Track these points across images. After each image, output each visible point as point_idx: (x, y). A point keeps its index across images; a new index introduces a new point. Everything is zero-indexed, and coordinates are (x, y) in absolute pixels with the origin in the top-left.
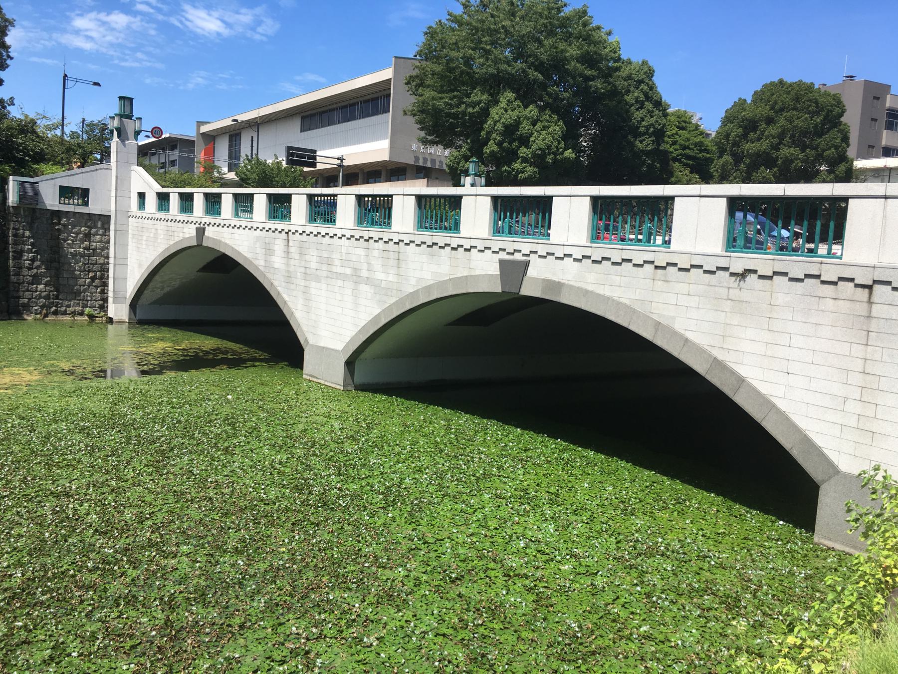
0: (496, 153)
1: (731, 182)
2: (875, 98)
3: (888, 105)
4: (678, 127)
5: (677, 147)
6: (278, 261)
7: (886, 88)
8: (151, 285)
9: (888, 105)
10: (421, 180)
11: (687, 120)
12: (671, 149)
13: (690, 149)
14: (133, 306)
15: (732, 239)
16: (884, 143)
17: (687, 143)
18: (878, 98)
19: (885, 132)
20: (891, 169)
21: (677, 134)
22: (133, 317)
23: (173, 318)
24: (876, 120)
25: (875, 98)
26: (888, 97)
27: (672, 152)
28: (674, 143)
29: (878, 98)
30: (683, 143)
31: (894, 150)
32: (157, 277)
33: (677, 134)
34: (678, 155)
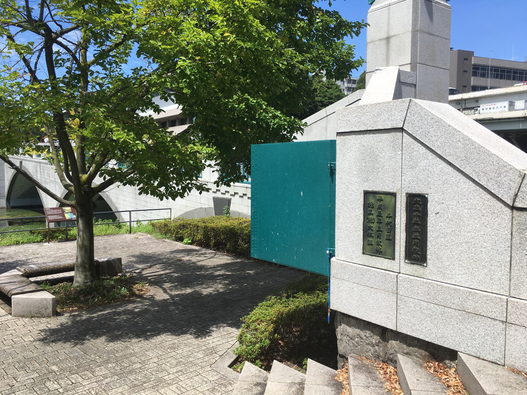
0: (108, 109)
1: (499, 159)
2: (465, 59)
3: (473, 63)
4: (327, 87)
5: (327, 98)
6: (39, 175)
7: (471, 53)
8: (14, 189)
9: (473, 63)
10: (522, 101)
11: (333, 83)
12: (323, 100)
13: (333, 99)
14: (8, 199)
15: (399, 373)
16: (472, 84)
17: (331, 96)
18: (467, 59)
19: (472, 78)
20: (465, 100)
21: (326, 91)
22: (8, 205)
23: (30, 204)
24: (466, 71)
25: (465, 59)
26: (473, 58)
27: (324, 101)
28: (325, 96)
29: (467, 59)
30: (329, 96)
31: (478, 88)
32: (15, 185)
33: (326, 91)
34: (327, 103)
